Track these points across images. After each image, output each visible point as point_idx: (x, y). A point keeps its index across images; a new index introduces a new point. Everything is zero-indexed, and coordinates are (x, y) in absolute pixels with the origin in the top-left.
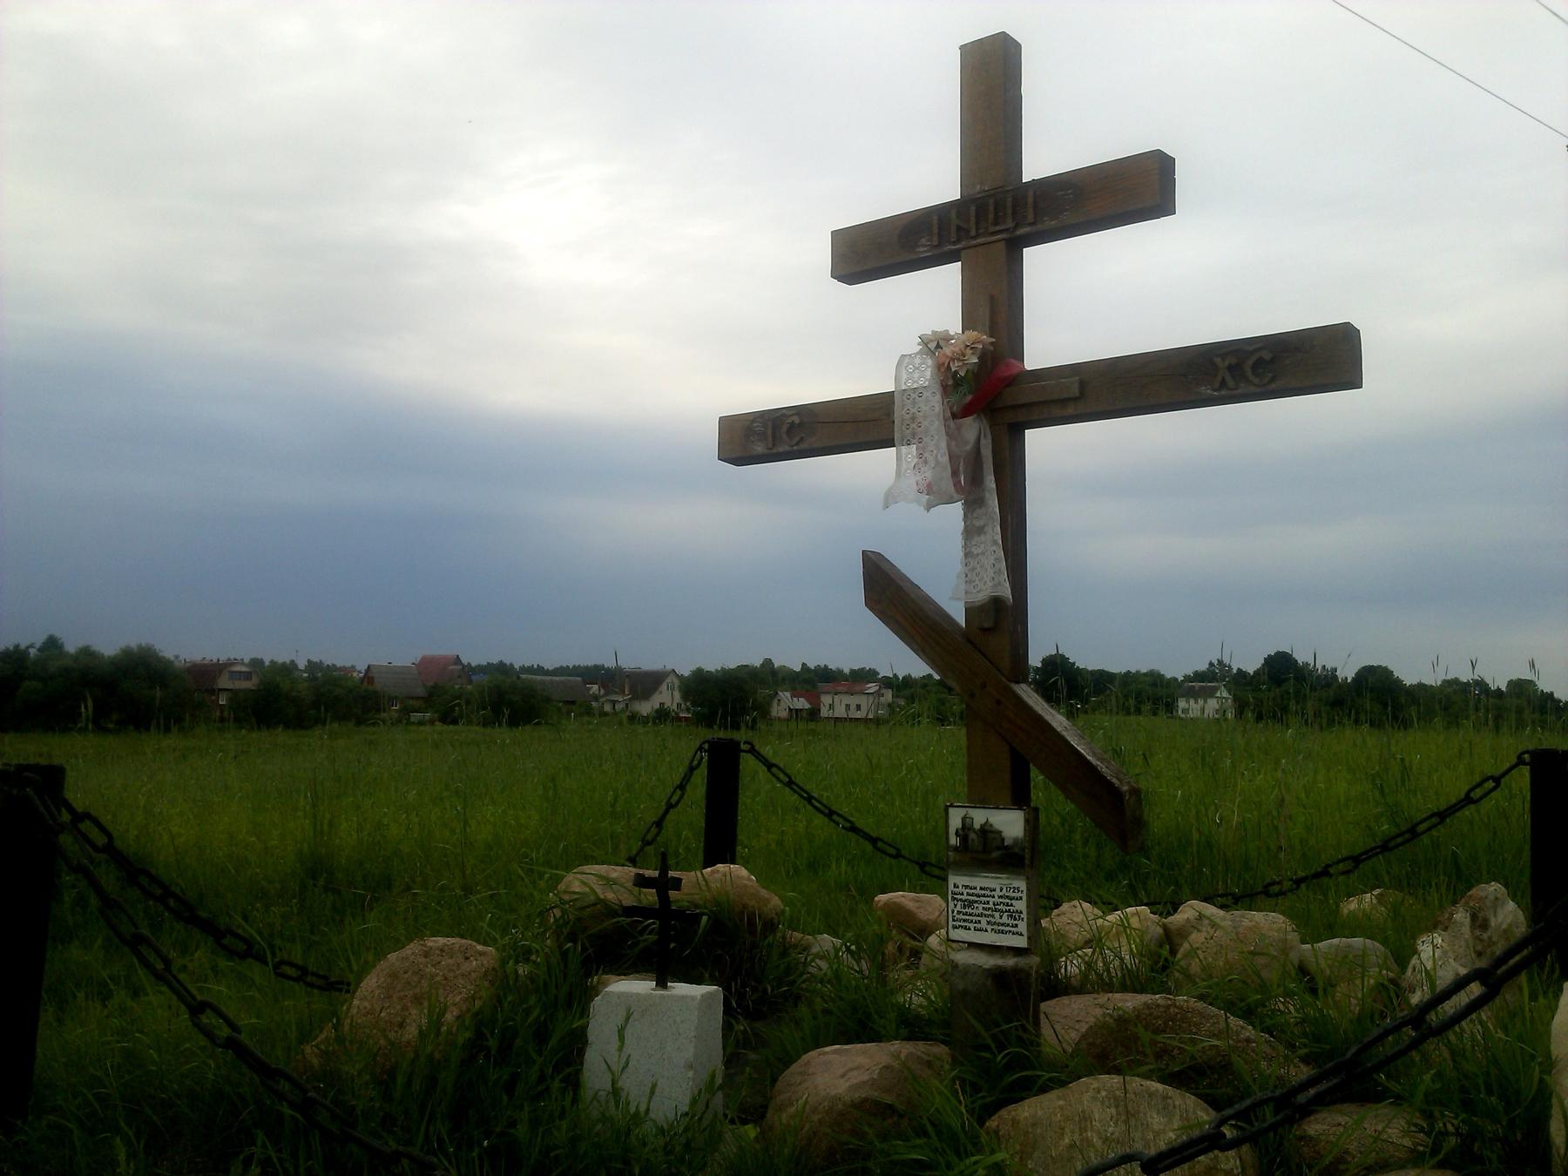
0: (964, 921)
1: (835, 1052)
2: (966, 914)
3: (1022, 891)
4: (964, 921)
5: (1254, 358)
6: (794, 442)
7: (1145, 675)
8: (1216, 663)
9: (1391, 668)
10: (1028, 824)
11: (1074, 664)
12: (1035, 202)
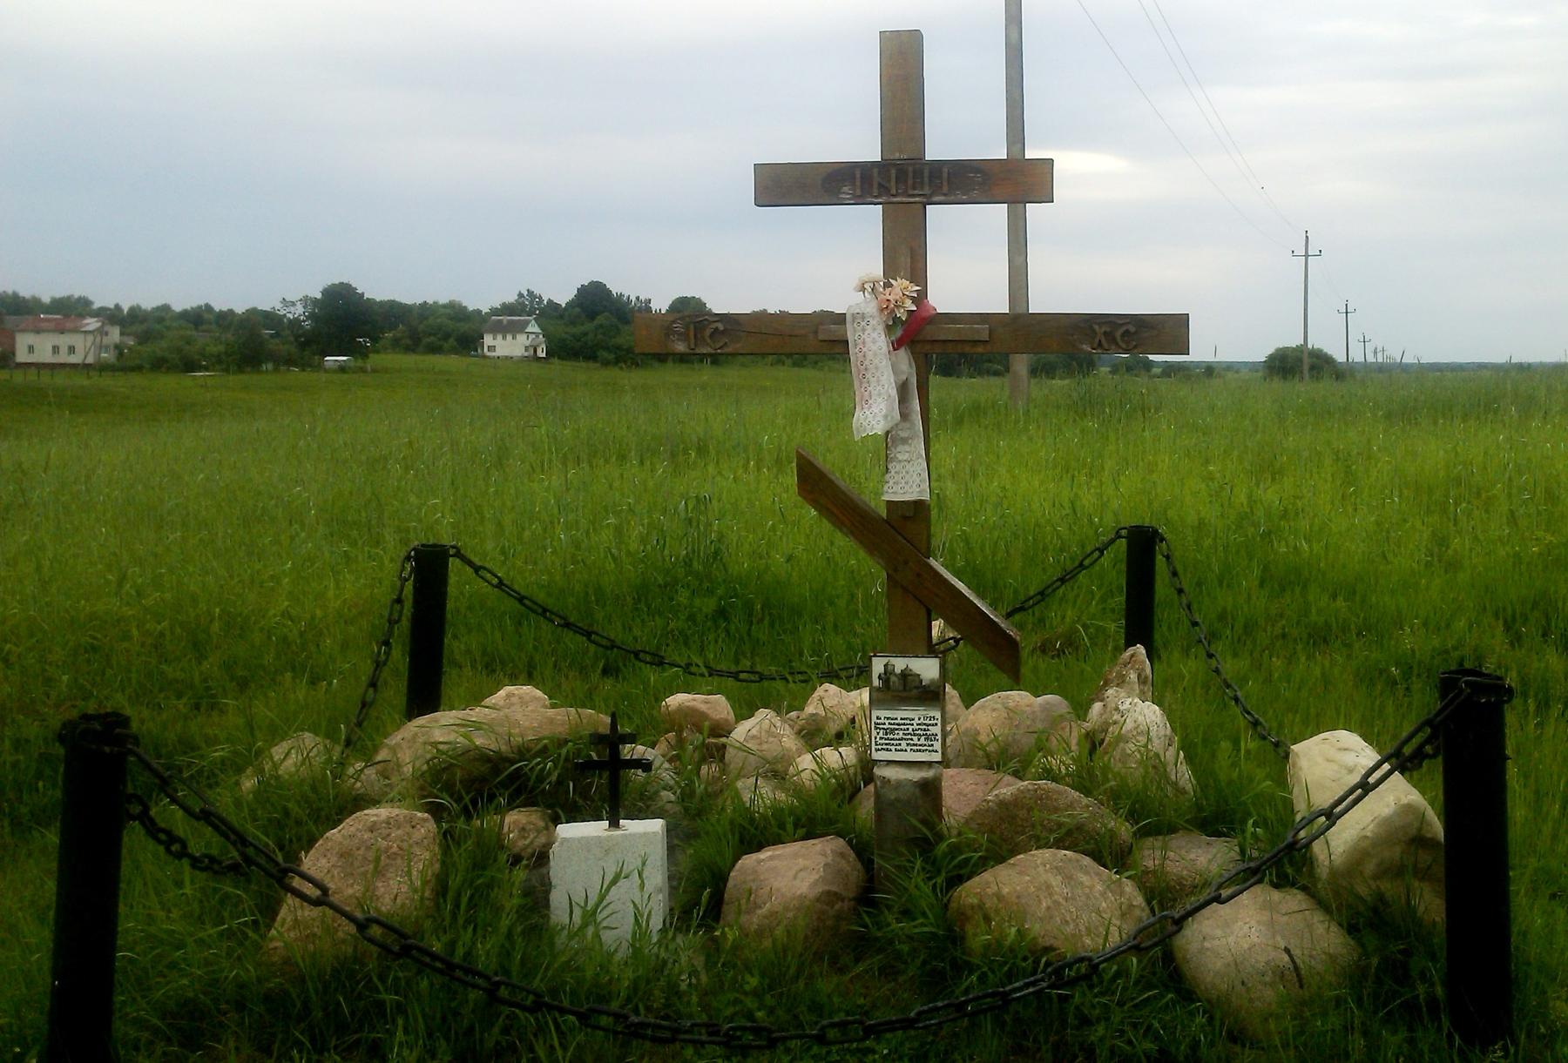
0: (886, 744)
1: (771, 858)
2: (888, 739)
4: (886, 744)
5: (1125, 328)
6: (718, 346)
7: (444, 306)
8: (525, 293)
9: (704, 300)
11: (363, 294)
12: (949, 178)
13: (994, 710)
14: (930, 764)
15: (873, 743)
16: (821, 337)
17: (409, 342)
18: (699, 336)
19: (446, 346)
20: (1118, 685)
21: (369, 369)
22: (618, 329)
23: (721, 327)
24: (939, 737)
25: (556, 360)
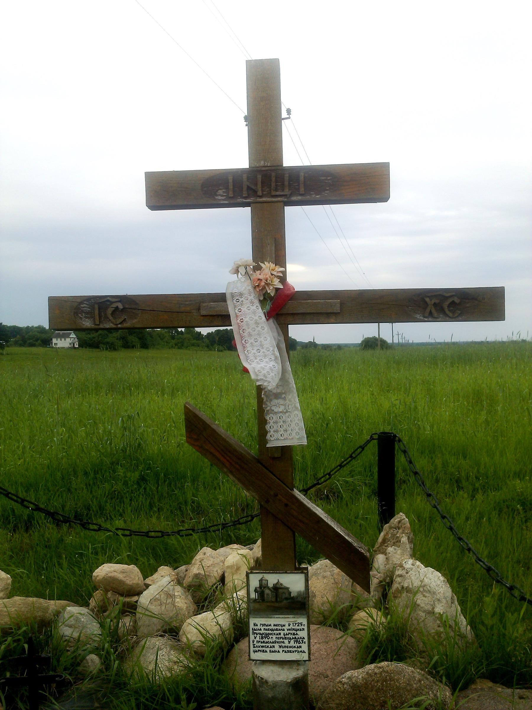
0: (262, 647)
4: (262, 647)
5: (451, 300)
6: (118, 322)
7: (36, 327)
13: (324, 577)
14: (297, 663)
15: (252, 646)
16: (203, 312)
17: (21, 342)
18: (103, 314)
19: (37, 343)
20: (394, 544)
21: (5, 354)
22: (107, 335)
23: (121, 306)
24: (306, 640)
25: (81, 348)
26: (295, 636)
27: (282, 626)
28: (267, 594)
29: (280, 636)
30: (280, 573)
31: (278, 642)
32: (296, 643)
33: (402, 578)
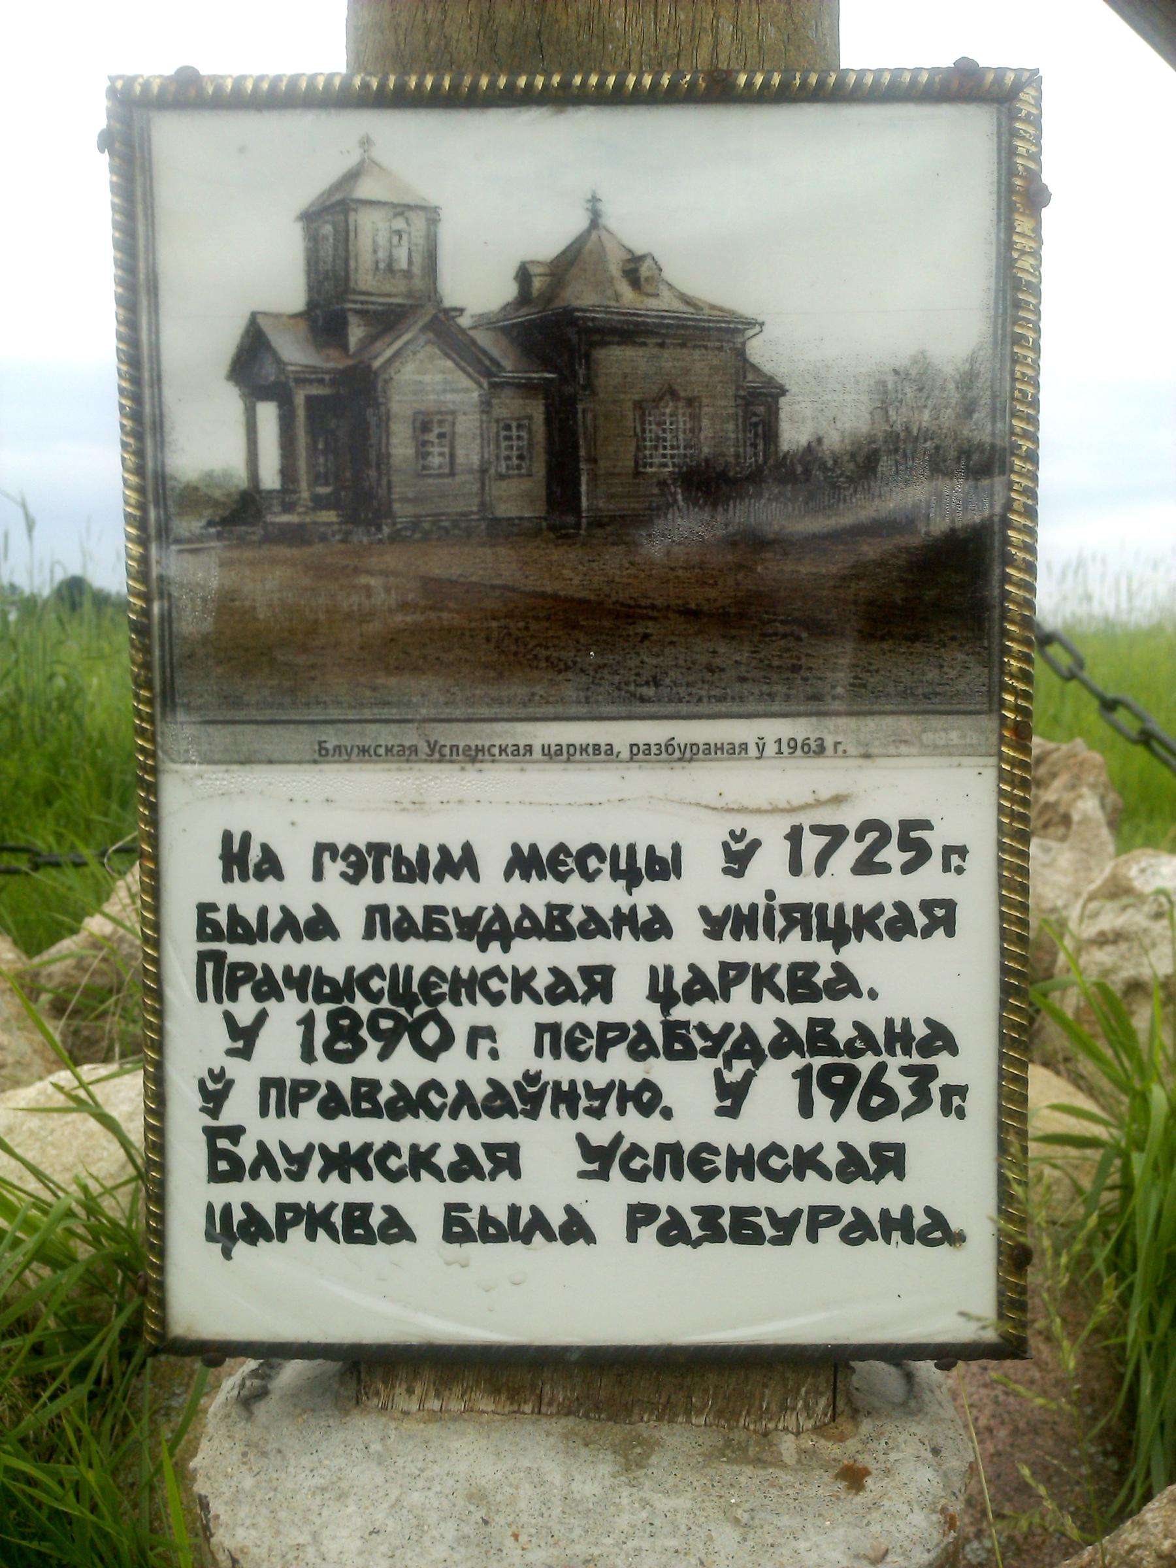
3: (955, 853)
10: (379, 455)
26: (824, 1008)
27: (632, 878)
28: (423, 424)
29: (593, 1013)
30: (617, 98)
31: (566, 1098)
32: (823, 1103)
33: (1123, 946)
